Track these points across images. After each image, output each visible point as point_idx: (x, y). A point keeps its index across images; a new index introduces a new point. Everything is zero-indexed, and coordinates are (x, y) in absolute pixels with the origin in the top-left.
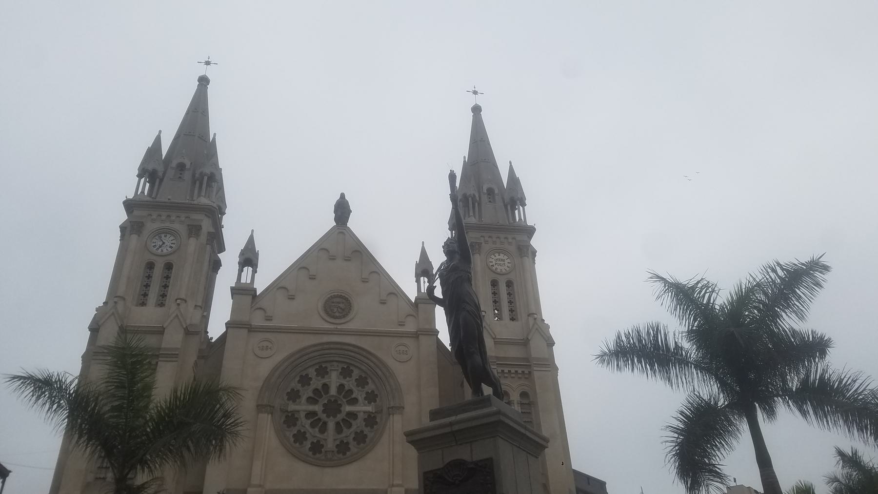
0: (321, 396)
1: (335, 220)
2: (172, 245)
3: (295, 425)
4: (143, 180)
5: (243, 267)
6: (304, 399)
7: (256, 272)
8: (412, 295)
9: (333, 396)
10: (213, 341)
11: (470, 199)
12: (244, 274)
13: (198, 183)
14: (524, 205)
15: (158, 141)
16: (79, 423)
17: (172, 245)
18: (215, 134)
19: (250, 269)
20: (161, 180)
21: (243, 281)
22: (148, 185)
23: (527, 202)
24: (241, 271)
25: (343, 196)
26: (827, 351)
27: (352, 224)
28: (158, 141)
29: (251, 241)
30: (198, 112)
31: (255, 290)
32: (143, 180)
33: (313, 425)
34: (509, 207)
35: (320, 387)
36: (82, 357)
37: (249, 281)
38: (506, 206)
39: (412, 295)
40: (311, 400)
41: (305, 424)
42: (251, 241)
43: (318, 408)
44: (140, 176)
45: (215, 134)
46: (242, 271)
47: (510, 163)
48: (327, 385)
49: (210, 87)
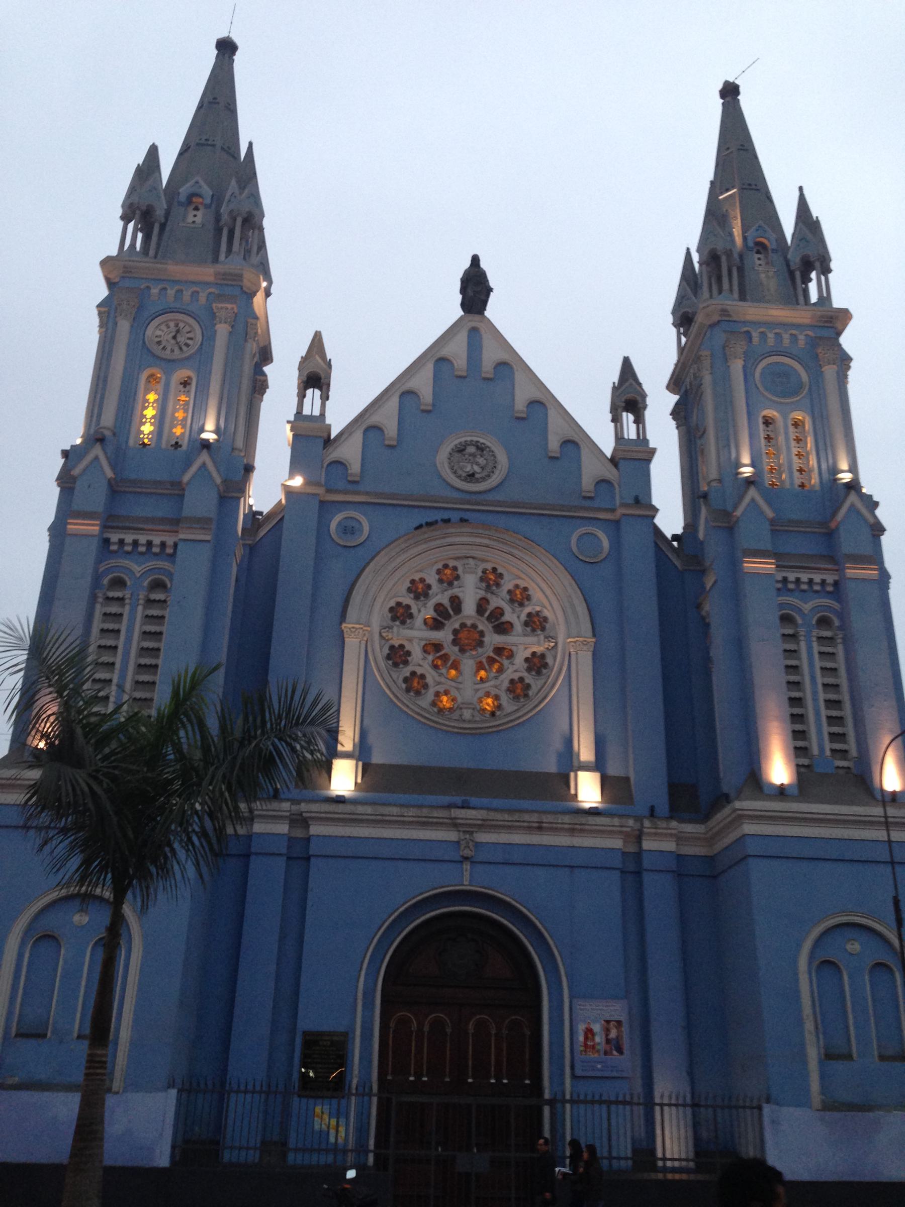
0: (448, 617)
1: (463, 305)
2: (189, 342)
3: (406, 663)
4: (131, 226)
5: (306, 388)
6: (419, 621)
7: (328, 398)
8: (607, 446)
9: (468, 617)
10: (283, 501)
11: (724, 259)
12: (307, 401)
13: (225, 232)
14: (826, 270)
15: (153, 152)
16: (449, 1034)
17: (189, 342)
18: (251, 144)
19: (318, 393)
20: (163, 227)
21: (306, 411)
22: (140, 236)
23: (833, 265)
24: (302, 396)
25: (475, 260)
26: (31, 632)
27: (494, 310)
28: (153, 152)
29: (317, 343)
30: (218, 103)
31: (329, 427)
32: (131, 226)
33: (499, 612)
34: (798, 274)
35: (446, 602)
36: (50, 529)
37: (316, 412)
38: (791, 274)
39: (607, 445)
40: (436, 625)
41: (420, 662)
42: (317, 343)
43: (444, 636)
44: (126, 218)
45: (251, 144)
46: (304, 396)
47: (801, 189)
48: (457, 597)
49: (238, 58)
